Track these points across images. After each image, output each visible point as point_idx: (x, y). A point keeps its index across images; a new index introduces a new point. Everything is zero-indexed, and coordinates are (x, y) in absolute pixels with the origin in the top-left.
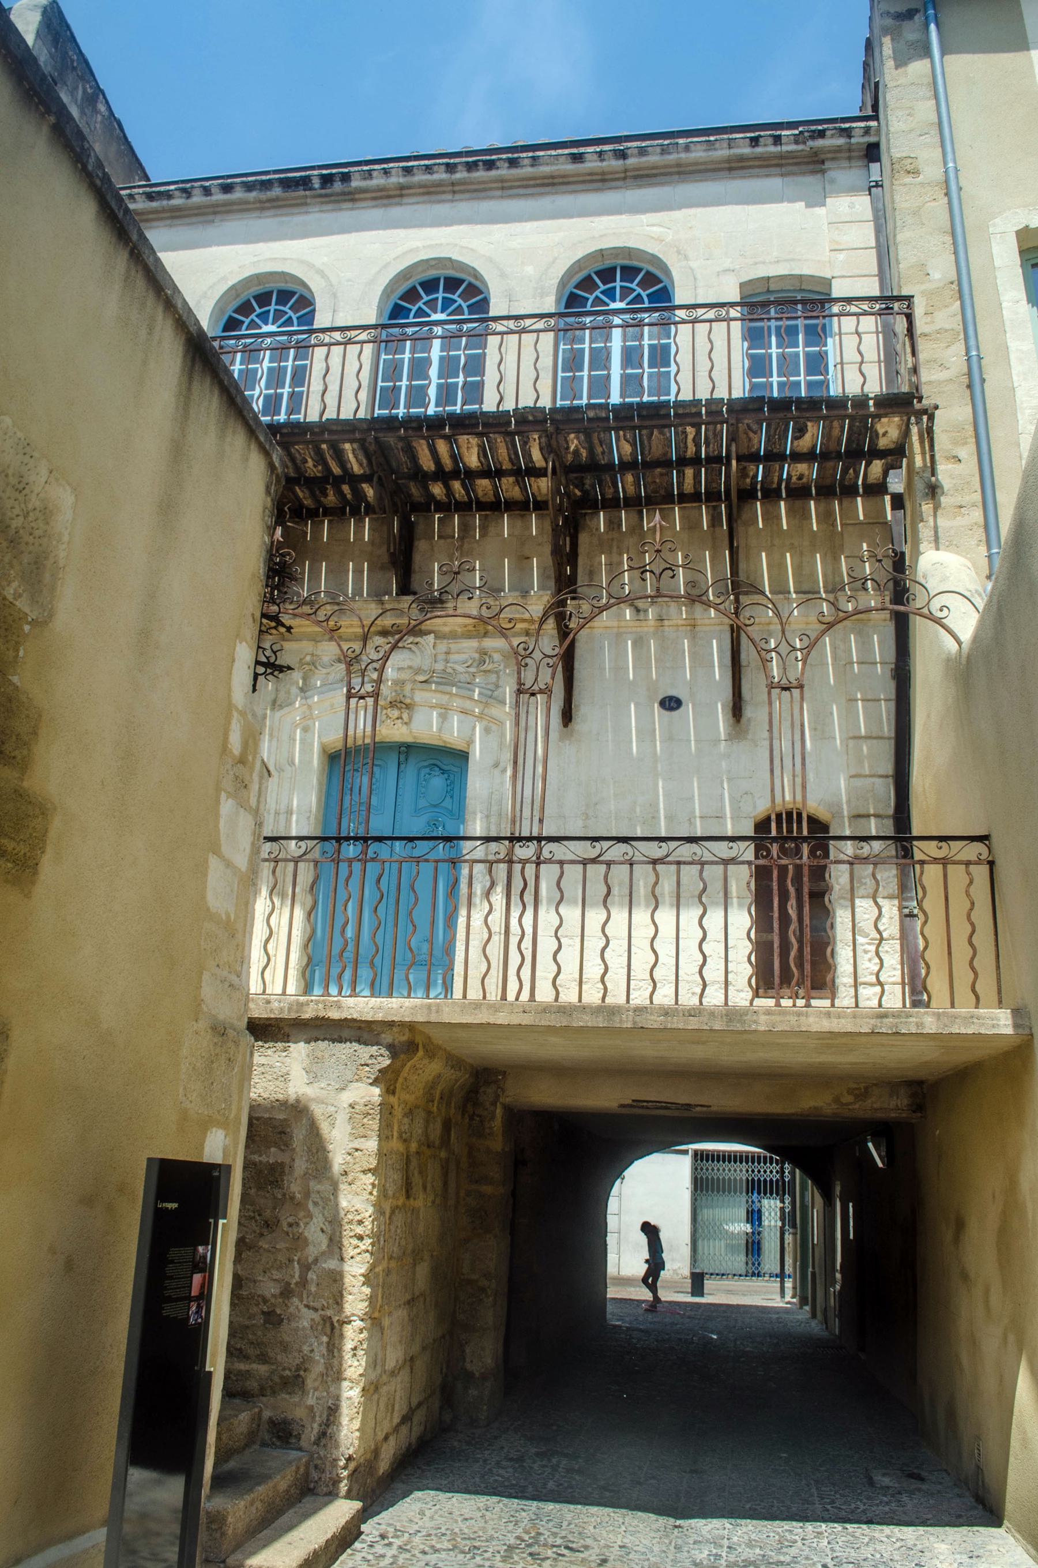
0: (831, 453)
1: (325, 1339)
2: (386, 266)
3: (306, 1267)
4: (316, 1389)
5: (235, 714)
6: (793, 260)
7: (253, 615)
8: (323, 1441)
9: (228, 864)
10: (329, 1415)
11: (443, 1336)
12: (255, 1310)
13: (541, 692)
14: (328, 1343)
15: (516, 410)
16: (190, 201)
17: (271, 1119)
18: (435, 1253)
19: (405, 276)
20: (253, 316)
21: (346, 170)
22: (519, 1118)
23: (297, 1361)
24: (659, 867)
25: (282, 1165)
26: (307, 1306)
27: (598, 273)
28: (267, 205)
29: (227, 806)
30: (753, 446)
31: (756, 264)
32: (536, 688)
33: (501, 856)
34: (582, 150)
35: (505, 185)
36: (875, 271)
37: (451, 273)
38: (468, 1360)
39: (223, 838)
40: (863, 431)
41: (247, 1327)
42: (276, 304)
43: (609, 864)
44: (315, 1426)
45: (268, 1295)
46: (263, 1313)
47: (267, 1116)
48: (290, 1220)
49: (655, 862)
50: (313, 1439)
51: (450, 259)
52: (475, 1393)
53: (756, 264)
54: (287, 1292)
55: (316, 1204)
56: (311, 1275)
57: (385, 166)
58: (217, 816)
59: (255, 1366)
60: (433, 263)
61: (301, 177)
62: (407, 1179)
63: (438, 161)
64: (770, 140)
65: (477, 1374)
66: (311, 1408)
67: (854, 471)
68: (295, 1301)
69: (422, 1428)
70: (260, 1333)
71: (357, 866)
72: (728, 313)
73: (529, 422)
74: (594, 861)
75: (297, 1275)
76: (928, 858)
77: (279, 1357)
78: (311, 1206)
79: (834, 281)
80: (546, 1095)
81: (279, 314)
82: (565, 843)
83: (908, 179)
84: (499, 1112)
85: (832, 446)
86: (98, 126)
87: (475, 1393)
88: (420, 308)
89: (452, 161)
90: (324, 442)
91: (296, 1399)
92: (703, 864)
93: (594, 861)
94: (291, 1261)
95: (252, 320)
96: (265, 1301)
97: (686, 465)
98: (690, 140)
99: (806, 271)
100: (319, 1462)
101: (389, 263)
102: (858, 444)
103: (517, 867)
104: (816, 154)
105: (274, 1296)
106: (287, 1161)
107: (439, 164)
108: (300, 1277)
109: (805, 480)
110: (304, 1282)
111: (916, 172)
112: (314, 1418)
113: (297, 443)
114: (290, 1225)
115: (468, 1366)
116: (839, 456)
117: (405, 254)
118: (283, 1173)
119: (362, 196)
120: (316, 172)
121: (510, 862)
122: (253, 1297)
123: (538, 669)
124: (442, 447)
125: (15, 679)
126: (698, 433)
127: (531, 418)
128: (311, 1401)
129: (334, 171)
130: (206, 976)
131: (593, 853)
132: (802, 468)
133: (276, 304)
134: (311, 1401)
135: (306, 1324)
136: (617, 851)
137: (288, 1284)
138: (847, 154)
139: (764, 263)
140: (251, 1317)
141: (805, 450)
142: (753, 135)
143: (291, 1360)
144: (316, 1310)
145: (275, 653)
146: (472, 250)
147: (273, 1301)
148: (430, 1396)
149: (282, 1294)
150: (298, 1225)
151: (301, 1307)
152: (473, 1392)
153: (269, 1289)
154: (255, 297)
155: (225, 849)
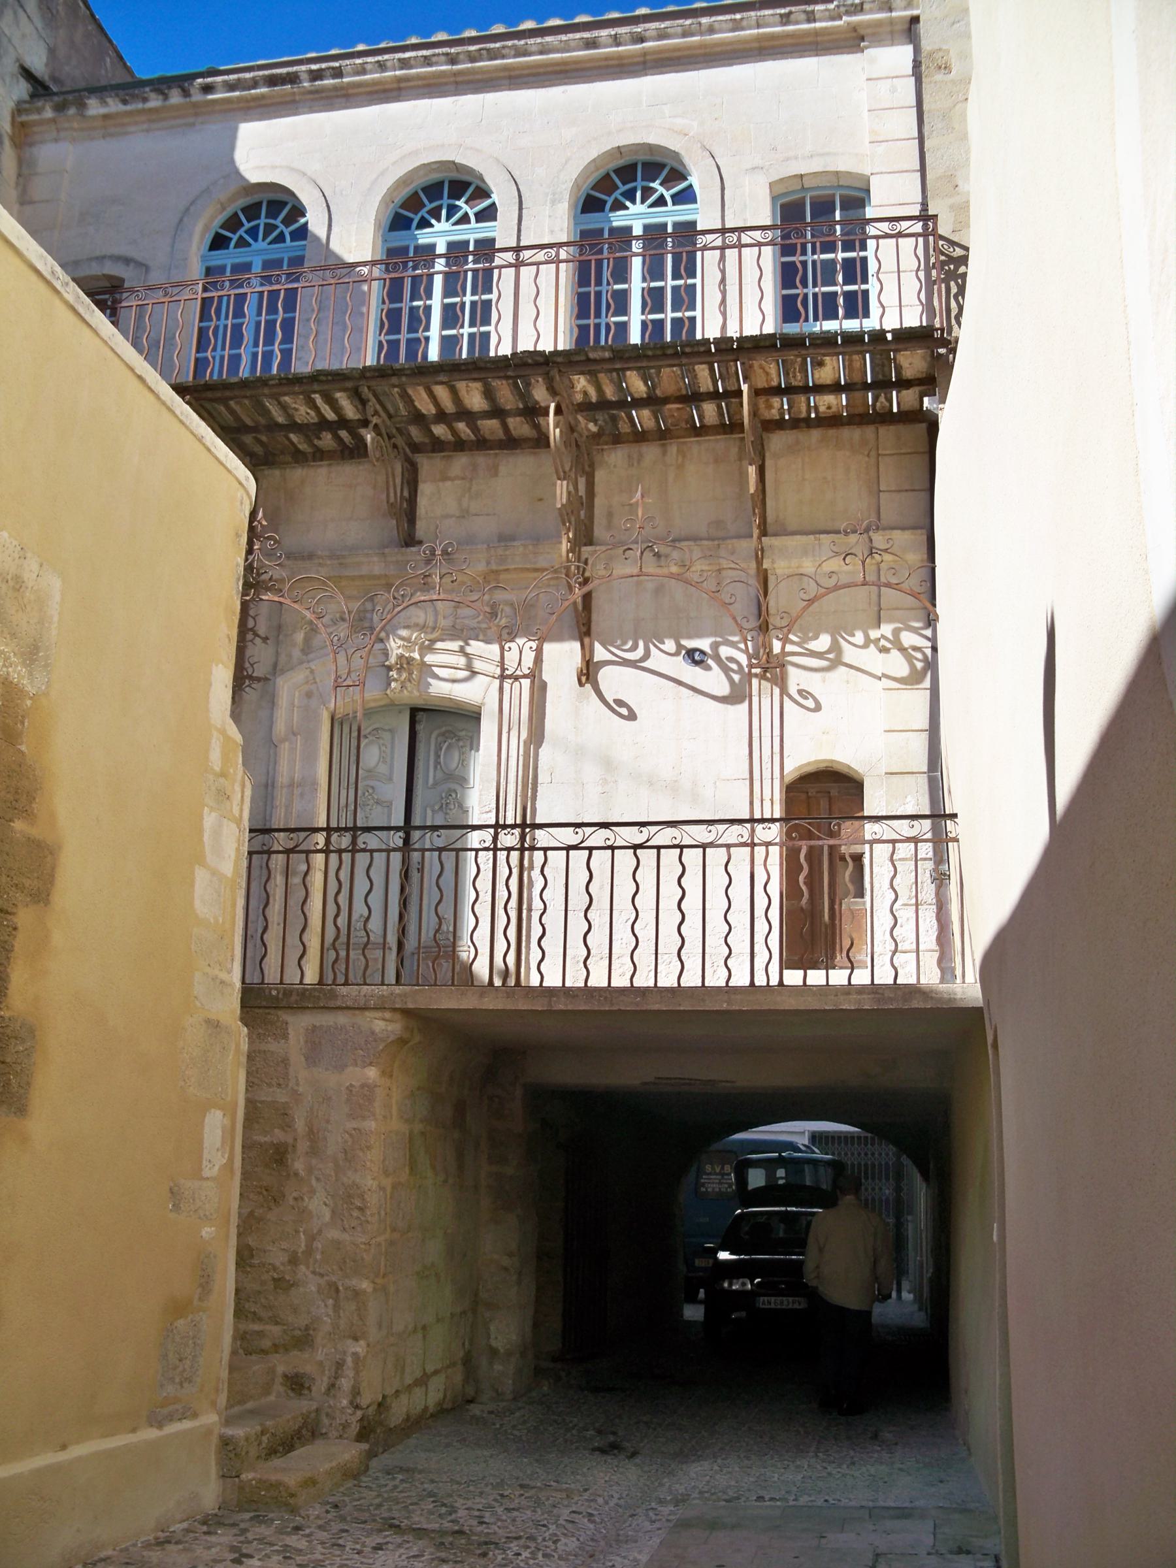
0: (855, 384)
1: (330, 1302)
2: (382, 174)
3: (312, 1238)
4: (324, 1346)
5: (215, 734)
6: (828, 154)
7: (228, 636)
8: (333, 1392)
9: (214, 872)
10: (337, 1368)
11: (464, 1313)
12: (265, 1277)
13: (525, 676)
14: (334, 1306)
15: (514, 354)
16: (167, 103)
17: (273, 1102)
18: (449, 1231)
19: (404, 182)
20: (241, 232)
21: (336, 64)
22: (541, 1097)
23: (306, 1322)
24: (639, 851)
25: (286, 1145)
26: (314, 1273)
27: (617, 171)
28: (252, 104)
29: (210, 820)
30: (772, 380)
31: (788, 159)
32: (518, 673)
33: (487, 845)
34: (595, 33)
35: (512, 73)
36: (918, 168)
37: (455, 175)
38: (493, 1336)
39: (207, 849)
40: (886, 362)
41: (259, 1292)
42: (266, 217)
43: (591, 849)
44: (325, 1379)
45: (278, 1264)
46: (274, 1279)
47: (269, 1099)
48: (295, 1194)
49: (635, 847)
50: (323, 1390)
51: (453, 162)
52: (501, 1368)
53: (788, 159)
54: (294, 1261)
55: (318, 1179)
56: (318, 1245)
57: (380, 58)
58: (200, 831)
59: (268, 1327)
60: (434, 166)
61: (288, 74)
62: (411, 1156)
63: (437, 51)
64: (803, 17)
65: (502, 1351)
66: (321, 1363)
67: (886, 398)
68: (303, 1268)
69: (441, 1395)
70: (271, 1298)
71: (346, 857)
72: (739, 239)
73: (530, 365)
74: (575, 847)
75: (303, 1245)
76: (899, 837)
77: (290, 1319)
78: (314, 1182)
79: (872, 179)
80: (567, 1073)
81: (270, 228)
82: (550, 830)
83: (939, 77)
84: (519, 1092)
85: (857, 378)
86: (60, 8)
87: (501, 1368)
88: (423, 217)
89: (453, 50)
90: (315, 392)
91: (306, 1356)
92: (681, 847)
93: (575, 847)
94: (297, 1232)
95: (241, 237)
96: (275, 1269)
97: (702, 401)
98: (713, 19)
99: (842, 167)
100: (330, 1410)
101: (387, 169)
102: (884, 375)
103: (502, 855)
104: (855, 29)
105: (283, 1264)
106: (290, 1141)
107: (439, 55)
108: (306, 1246)
109: (834, 409)
110: (309, 1251)
111: (947, 68)
112: (323, 1371)
113: (285, 394)
114: (296, 1199)
115: (494, 1343)
116: (866, 387)
117: (403, 158)
118: (286, 1151)
119: (356, 91)
120: (303, 68)
121: (495, 850)
122: (264, 1265)
123: (521, 652)
124: (441, 392)
125: (23, 748)
126: (712, 370)
127: (530, 361)
128: (320, 1356)
129: (324, 66)
130: (198, 975)
131: (574, 840)
132: (830, 399)
133: (266, 217)
134: (320, 1356)
135: (313, 1288)
136: (598, 837)
137: (295, 1252)
138: (889, 29)
139: (796, 158)
140: (263, 1283)
141: (829, 382)
142: (783, 11)
143: (302, 1321)
144: (322, 1275)
145: (252, 665)
146: (477, 150)
147: (282, 1268)
148: (448, 1367)
149: (290, 1262)
150: (302, 1199)
151: (308, 1273)
152: (498, 1367)
153: (277, 1257)
154: (243, 210)
155: (210, 857)
